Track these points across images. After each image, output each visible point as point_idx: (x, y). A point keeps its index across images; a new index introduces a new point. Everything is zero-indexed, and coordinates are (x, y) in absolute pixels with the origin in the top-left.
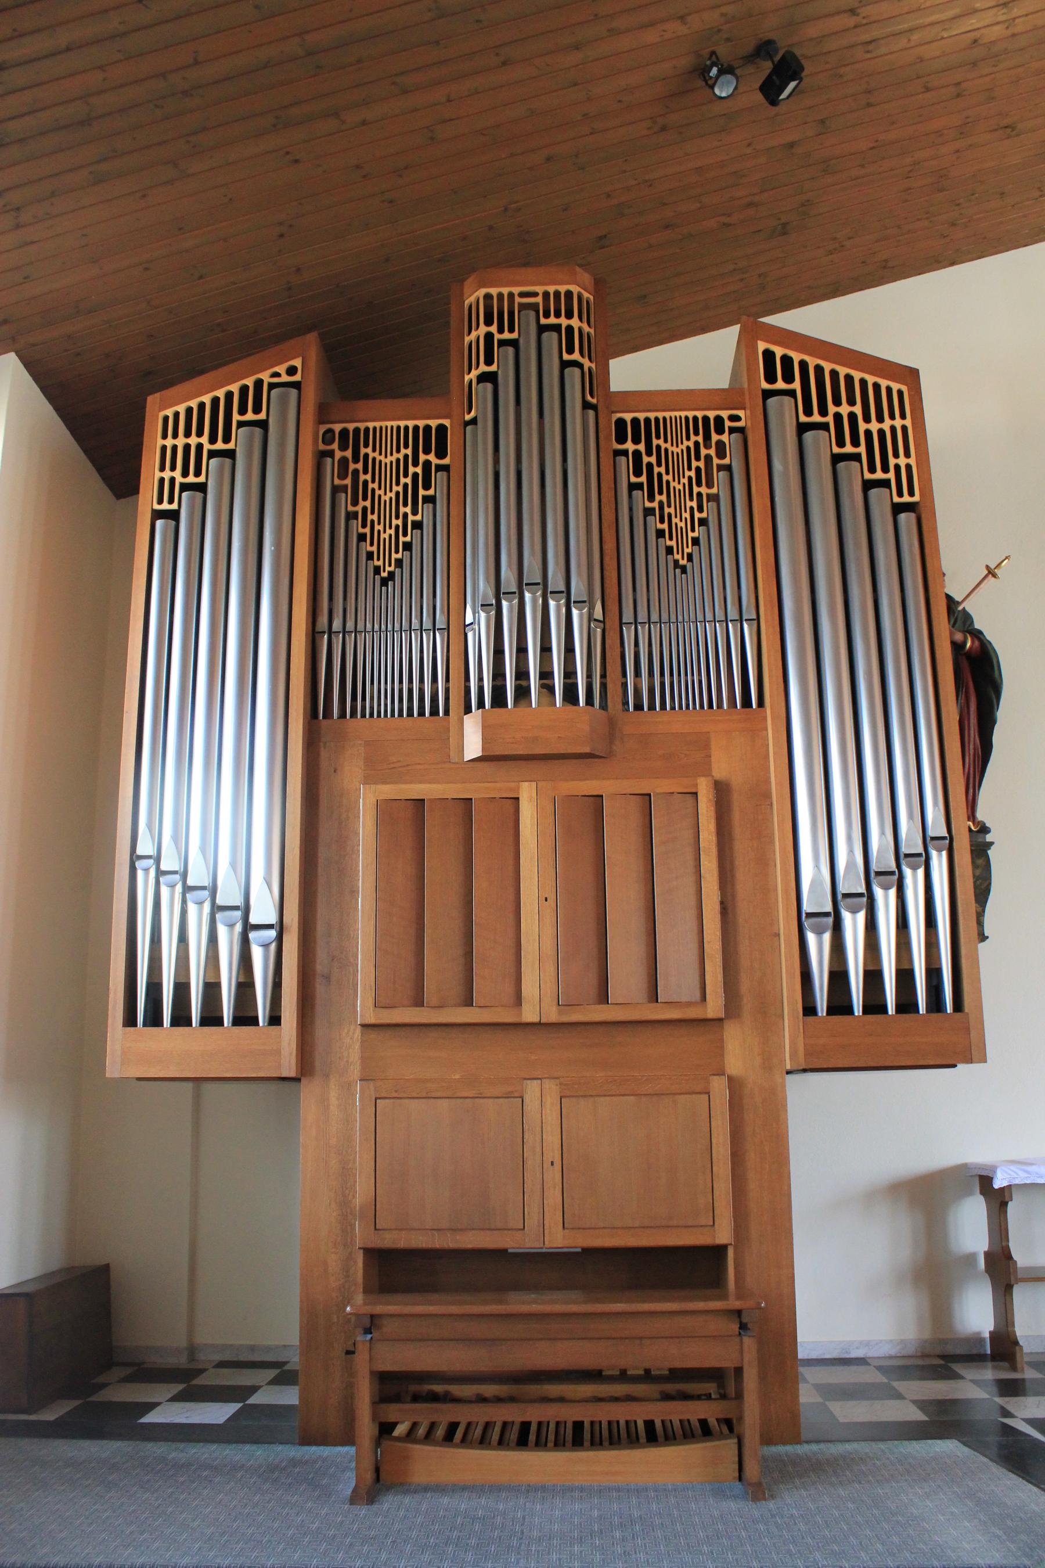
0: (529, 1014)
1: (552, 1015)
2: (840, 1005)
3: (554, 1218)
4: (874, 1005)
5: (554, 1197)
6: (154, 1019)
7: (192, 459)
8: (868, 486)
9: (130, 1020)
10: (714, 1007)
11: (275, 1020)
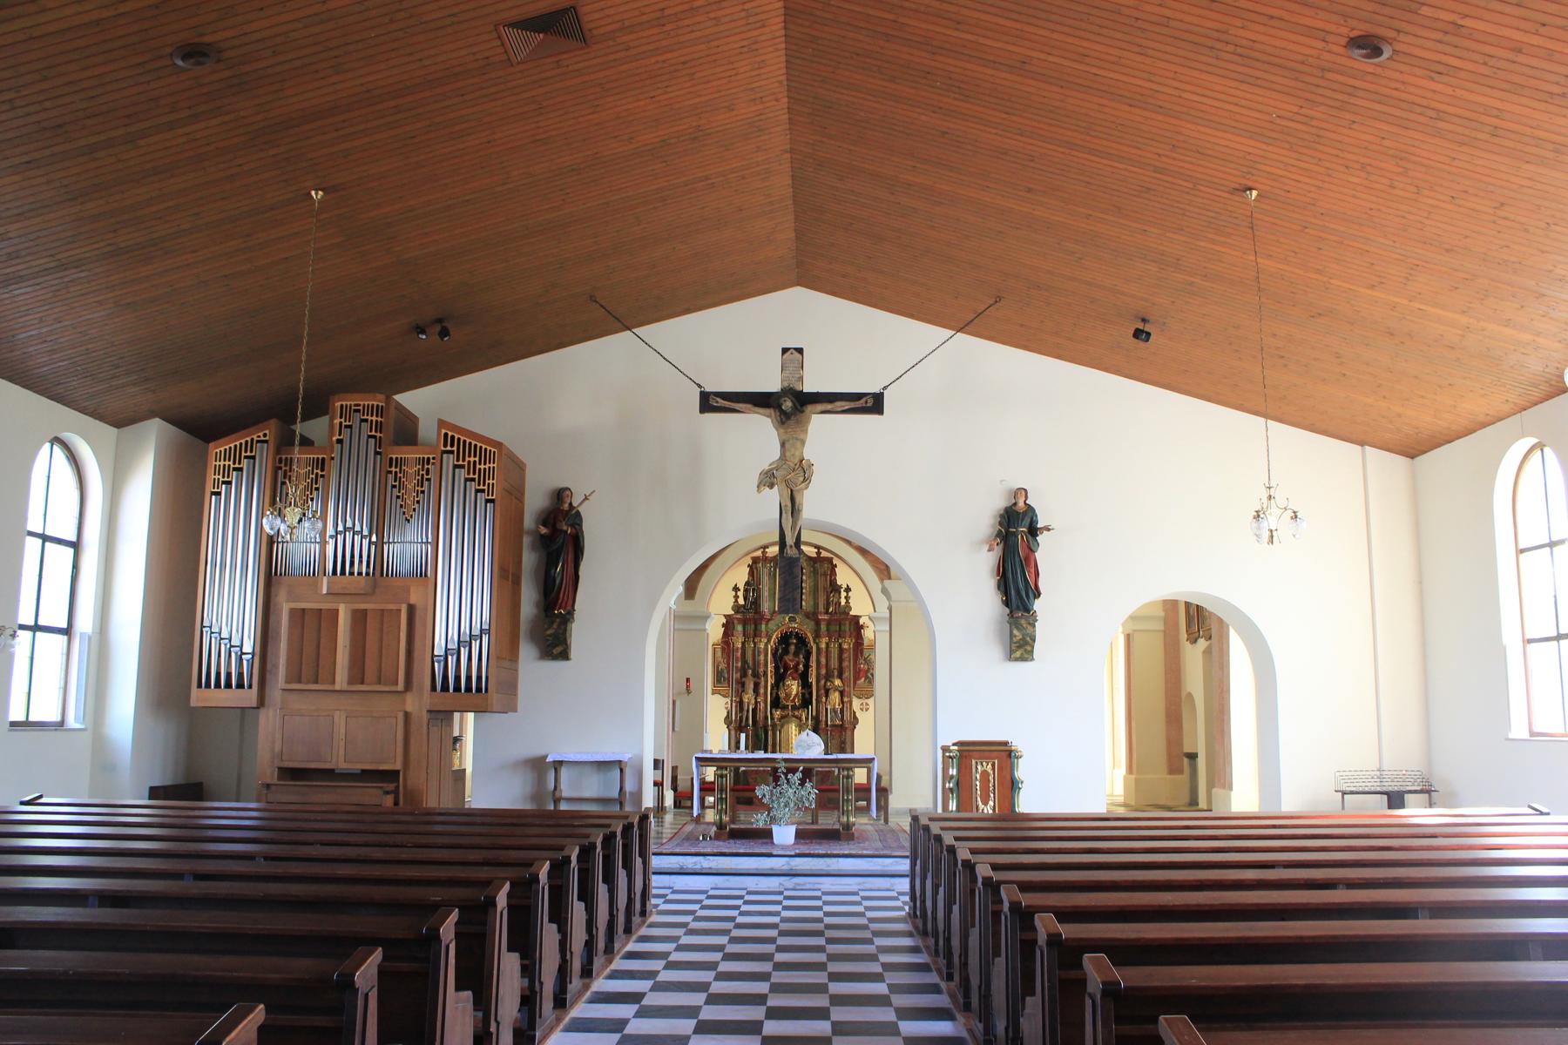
0: (337, 687)
1: (345, 687)
2: (445, 688)
3: (341, 759)
4: (457, 689)
5: (342, 752)
6: (208, 685)
7: (226, 471)
8: (477, 491)
9: (200, 686)
10: (401, 687)
11: (250, 686)
